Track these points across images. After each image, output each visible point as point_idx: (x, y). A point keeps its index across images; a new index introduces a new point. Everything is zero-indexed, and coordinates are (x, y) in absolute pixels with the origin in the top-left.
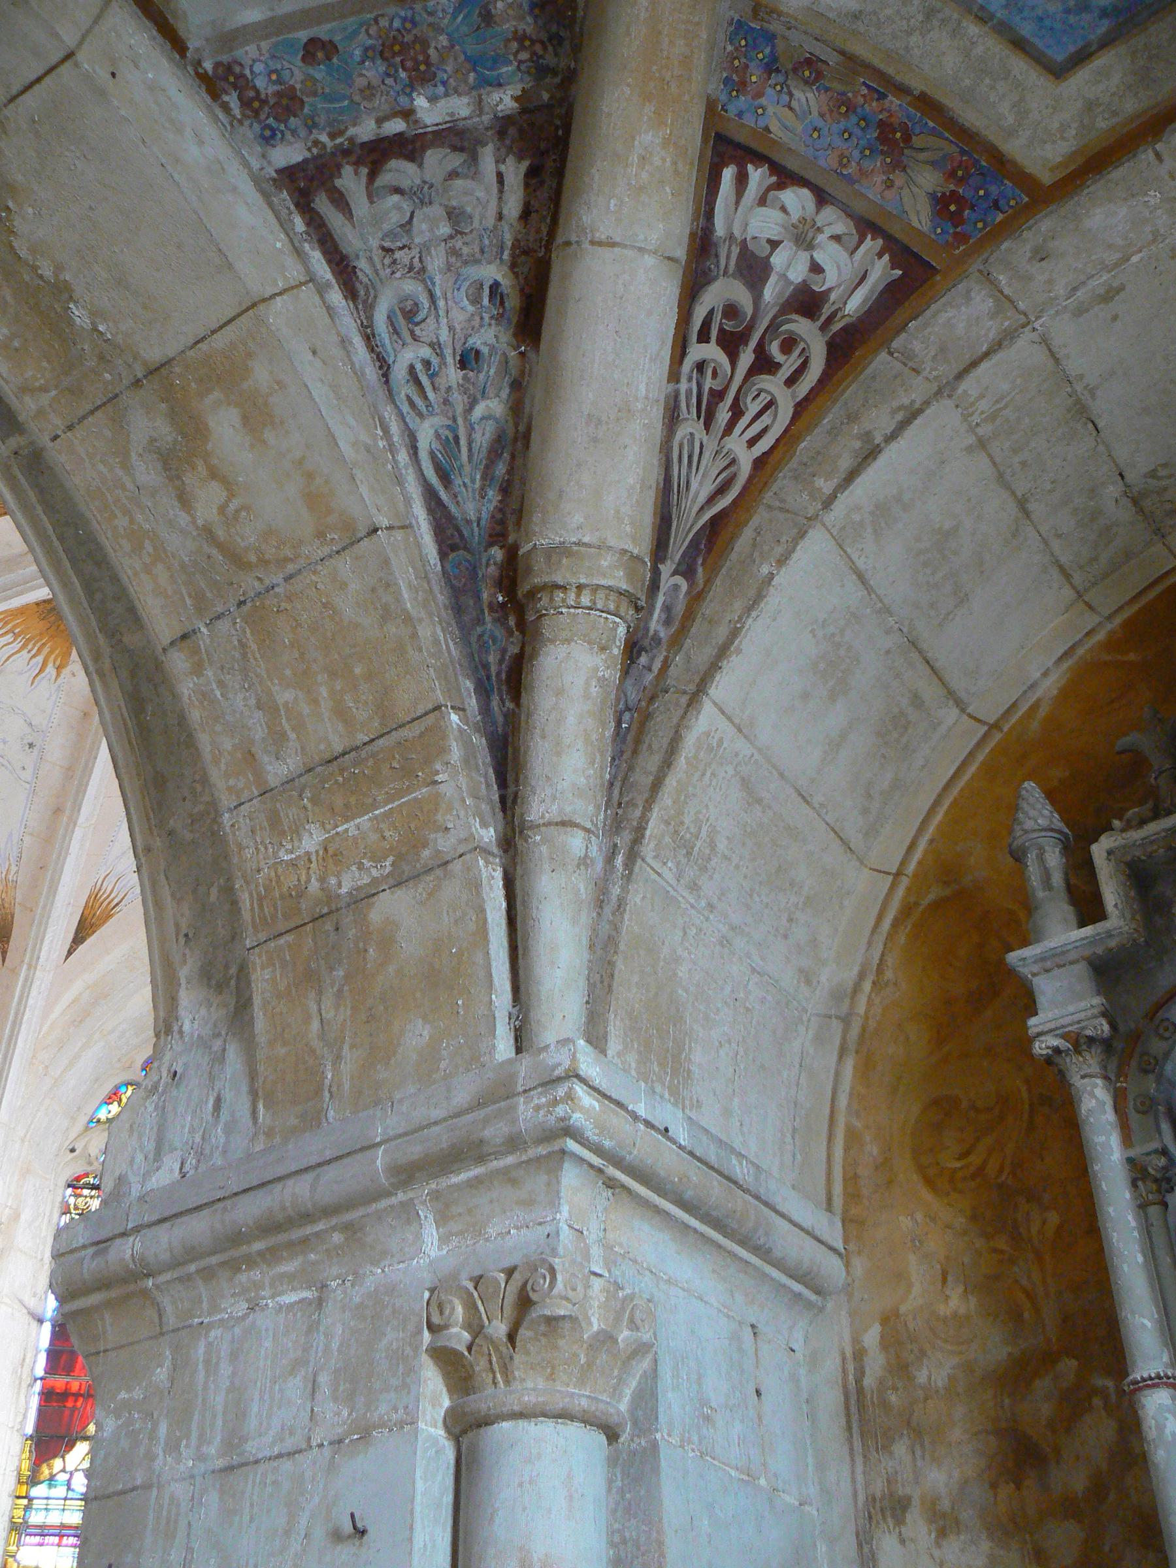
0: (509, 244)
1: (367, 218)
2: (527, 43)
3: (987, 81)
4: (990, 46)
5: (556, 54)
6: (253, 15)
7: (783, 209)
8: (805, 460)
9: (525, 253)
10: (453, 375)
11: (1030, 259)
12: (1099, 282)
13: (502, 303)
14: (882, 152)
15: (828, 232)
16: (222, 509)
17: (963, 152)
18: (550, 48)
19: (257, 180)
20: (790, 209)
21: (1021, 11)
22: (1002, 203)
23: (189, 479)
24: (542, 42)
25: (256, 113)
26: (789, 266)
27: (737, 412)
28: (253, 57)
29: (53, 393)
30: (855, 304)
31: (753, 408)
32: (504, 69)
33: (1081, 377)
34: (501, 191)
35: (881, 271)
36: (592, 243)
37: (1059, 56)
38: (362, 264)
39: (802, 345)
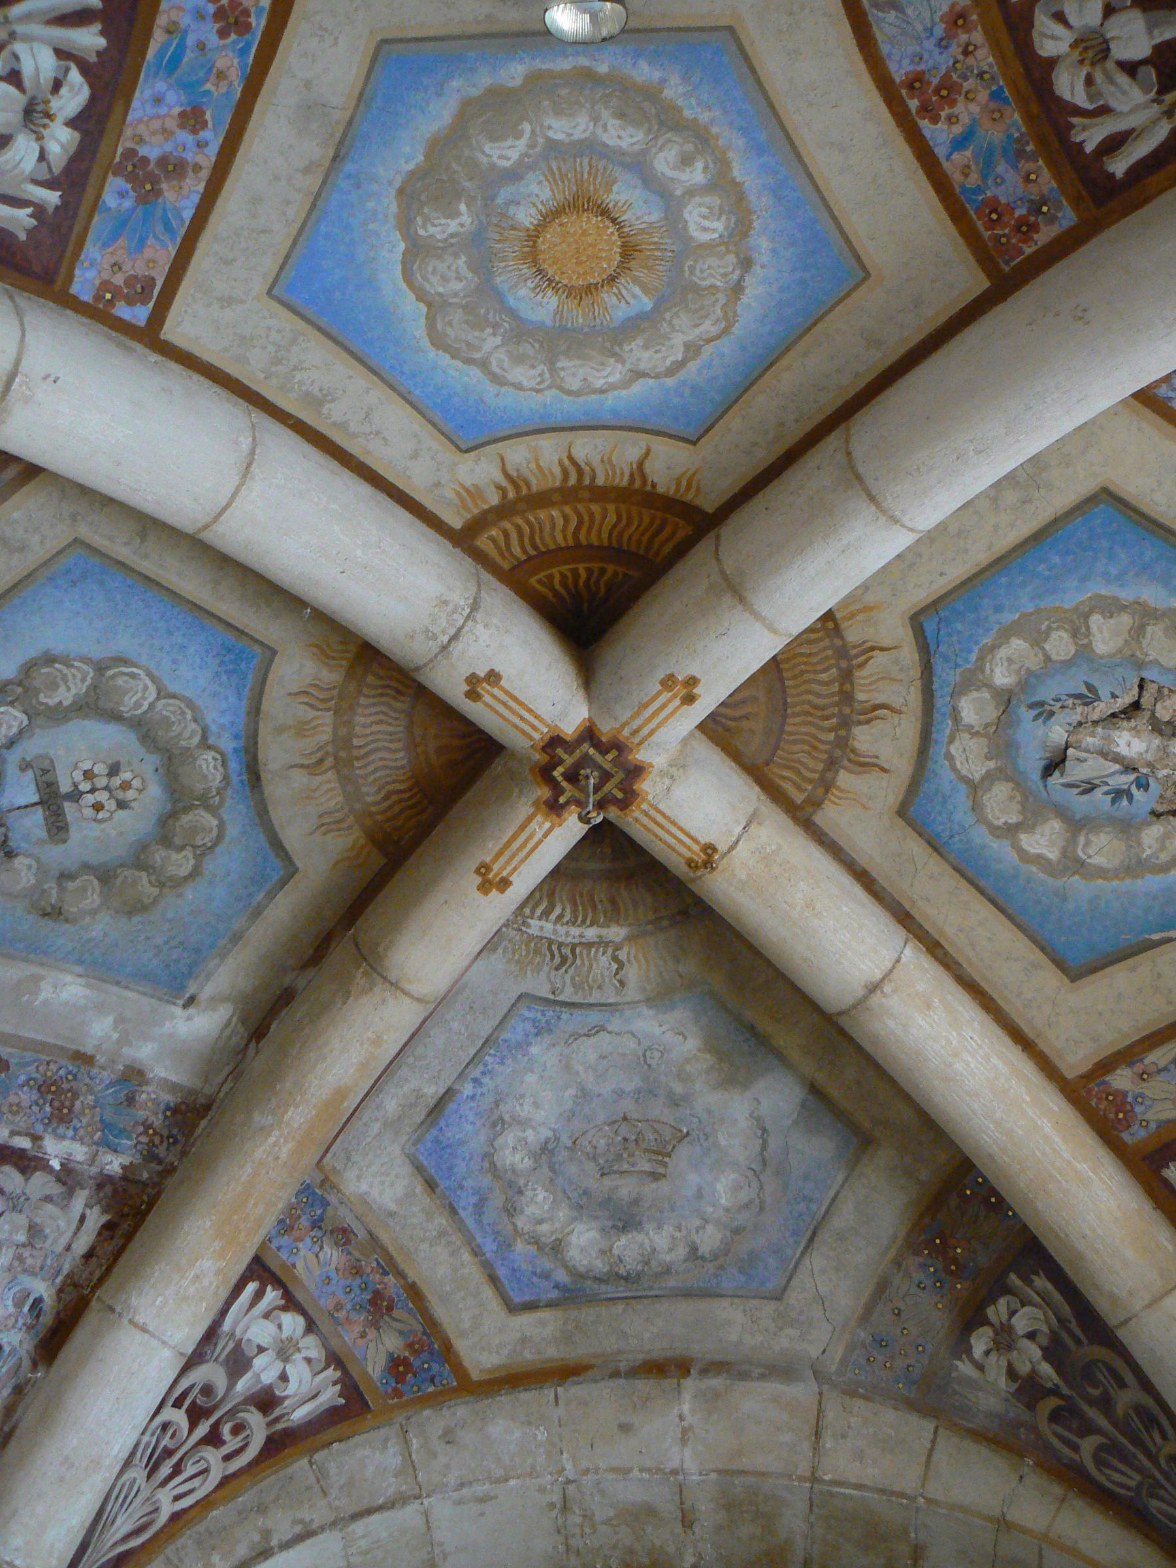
0: (65, 1272)
2: (151, 1132)
3: (462, 1294)
4: (473, 1272)
5: (168, 1149)
7: (280, 1327)
8: (212, 1529)
9: (75, 1285)
11: (439, 1438)
12: (480, 1489)
13: (38, 1316)
14: (369, 1311)
15: (305, 1353)
17: (425, 1333)
18: (165, 1144)
20: (284, 1327)
21: (503, 1259)
22: (437, 1380)
24: (161, 1136)
26: (265, 1370)
27: (177, 1470)
30: (300, 1414)
31: (190, 1470)
32: (124, 1141)
33: (442, 1544)
34: (78, 1229)
36: (131, 1322)
37: (517, 1299)
39: (248, 1432)
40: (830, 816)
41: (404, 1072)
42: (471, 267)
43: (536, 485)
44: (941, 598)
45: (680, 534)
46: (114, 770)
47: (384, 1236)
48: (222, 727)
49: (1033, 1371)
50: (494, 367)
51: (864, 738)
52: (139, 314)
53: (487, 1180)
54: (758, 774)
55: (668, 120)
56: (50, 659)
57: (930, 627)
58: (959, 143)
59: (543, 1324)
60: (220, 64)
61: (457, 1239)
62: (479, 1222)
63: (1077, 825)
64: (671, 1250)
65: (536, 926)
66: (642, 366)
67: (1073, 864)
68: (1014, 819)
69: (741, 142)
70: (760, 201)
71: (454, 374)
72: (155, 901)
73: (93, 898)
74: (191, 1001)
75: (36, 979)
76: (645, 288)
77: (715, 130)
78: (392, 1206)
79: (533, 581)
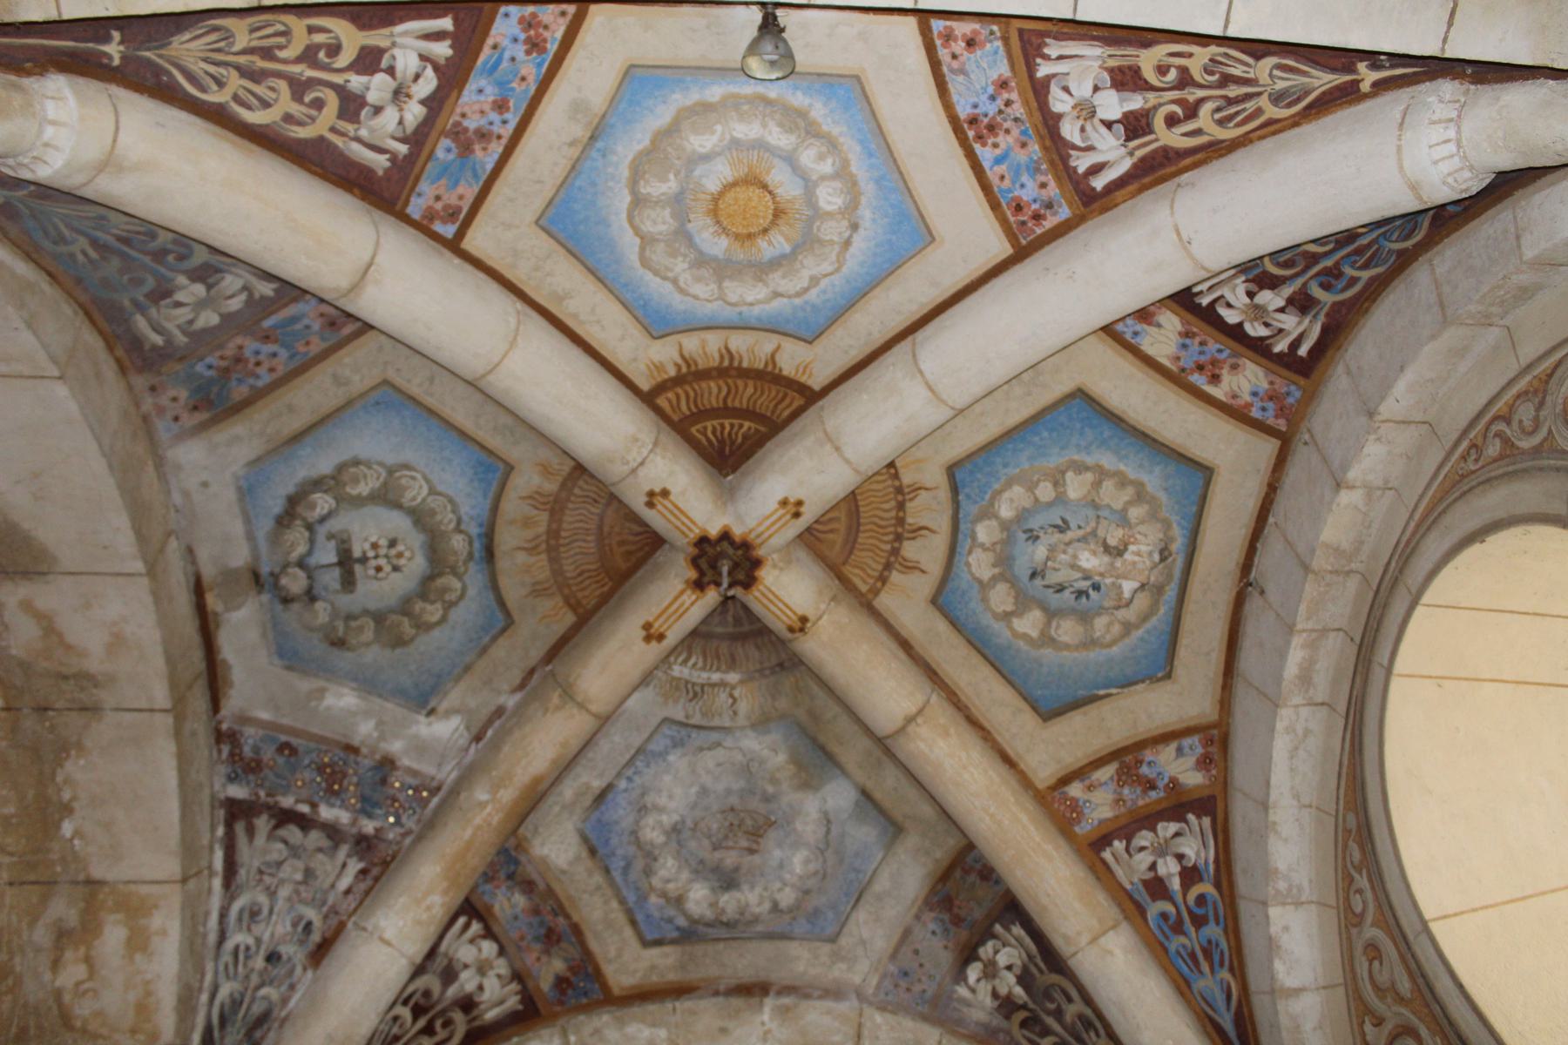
1: (259, 848)
4: (619, 917)
6: (265, 715)
7: (480, 950)
10: (259, 963)
15: (497, 971)
16: (78, 984)
19: (213, 797)
23: (69, 955)
25: (234, 762)
28: (250, 735)
29: (15, 859)
30: (491, 1015)
35: (513, 1003)
37: (649, 937)
38: (242, 872)
40: (885, 601)
41: (579, 769)
42: (673, 215)
43: (702, 364)
44: (970, 456)
45: (796, 404)
46: (393, 543)
47: (557, 888)
48: (472, 518)
49: (1010, 993)
50: (682, 284)
51: (910, 550)
52: (448, 231)
53: (632, 849)
54: (836, 571)
55: (812, 131)
56: (356, 462)
57: (959, 476)
58: (998, 161)
59: (666, 955)
60: (524, 72)
61: (609, 892)
62: (626, 881)
63: (1051, 614)
64: (759, 904)
65: (678, 671)
66: (780, 290)
67: (1046, 639)
68: (1009, 608)
69: (858, 148)
70: (868, 189)
71: (656, 287)
72: (412, 640)
73: (368, 635)
74: (431, 712)
75: (321, 692)
76: (787, 239)
77: (841, 140)
78: (565, 867)
79: (693, 430)
